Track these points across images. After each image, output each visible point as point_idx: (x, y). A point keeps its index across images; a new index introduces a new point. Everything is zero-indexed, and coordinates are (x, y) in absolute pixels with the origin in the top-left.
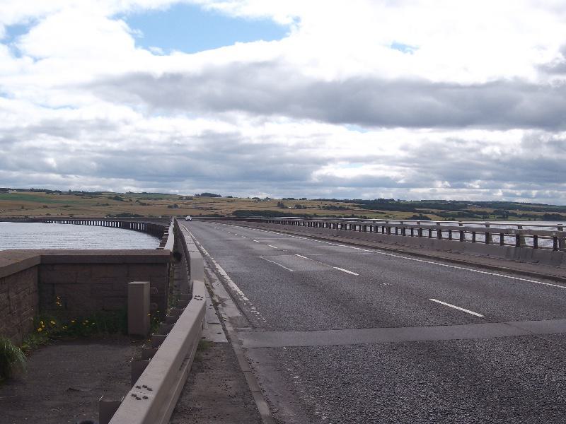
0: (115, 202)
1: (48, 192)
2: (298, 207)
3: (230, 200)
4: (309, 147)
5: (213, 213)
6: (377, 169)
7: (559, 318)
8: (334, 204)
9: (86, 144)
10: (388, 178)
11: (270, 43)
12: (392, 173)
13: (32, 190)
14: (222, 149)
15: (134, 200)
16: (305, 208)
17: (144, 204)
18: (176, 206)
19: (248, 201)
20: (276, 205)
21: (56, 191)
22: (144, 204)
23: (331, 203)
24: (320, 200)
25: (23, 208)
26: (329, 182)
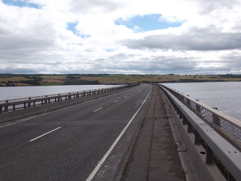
0: (142, 77)
1: (122, 75)
2: (200, 77)
3: (178, 76)
4: (195, 58)
5: (219, 80)
6: (218, 64)
7: (100, 120)
8: (212, 76)
9: (124, 62)
10: (26, 68)
11: (127, 28)
12: (217, 66)
13: (117, 75)
14: (164, 60)
15: (148, 76)
16: (203, 78)
17: (150, 78)
18: (161, 78)
19: (183, 76)
20: (193, 77)
21: (124, 75)
22: (150, 78)
23: (211, 76)
24: (207, 75)
25: (113, 80)
26: (201, 69)
